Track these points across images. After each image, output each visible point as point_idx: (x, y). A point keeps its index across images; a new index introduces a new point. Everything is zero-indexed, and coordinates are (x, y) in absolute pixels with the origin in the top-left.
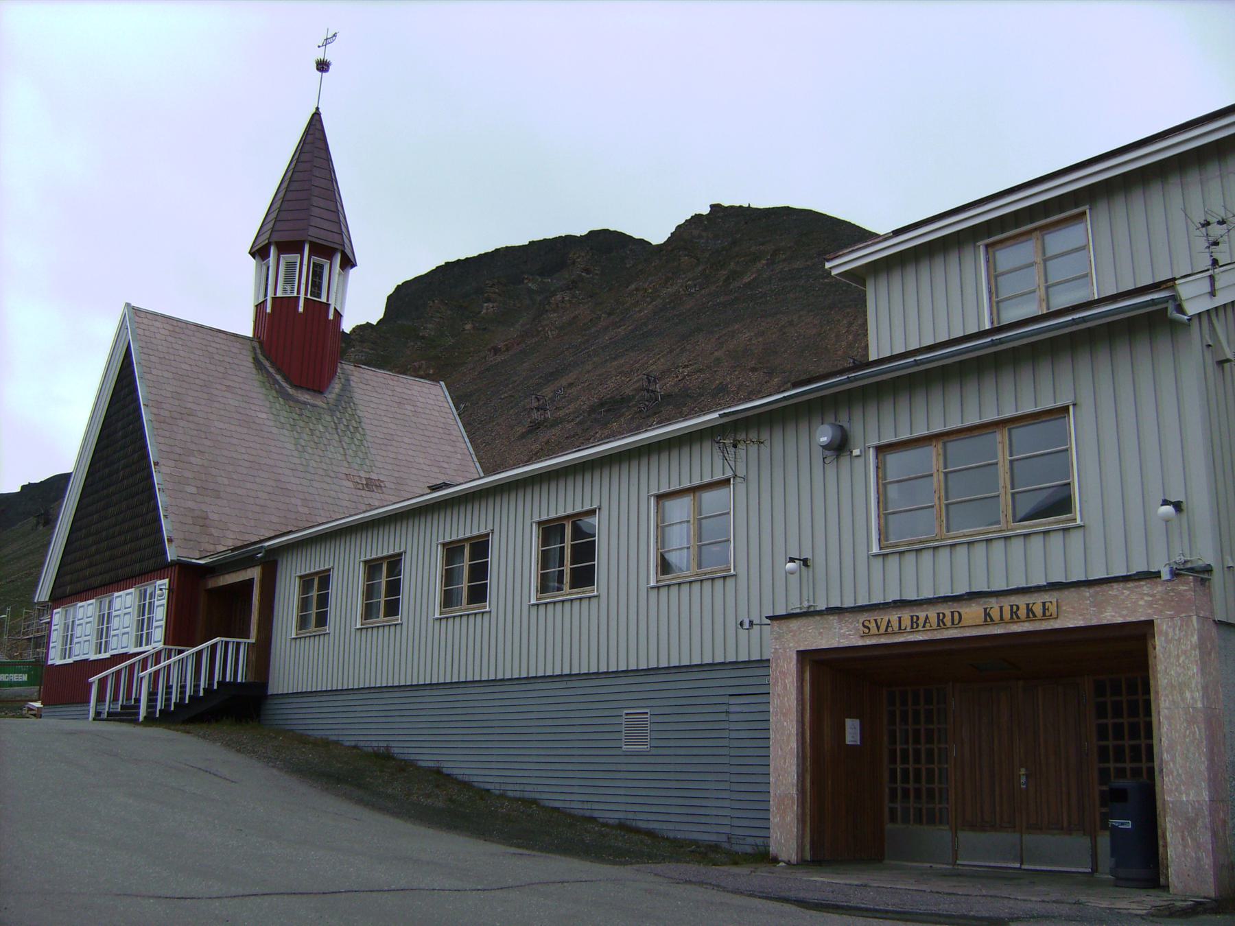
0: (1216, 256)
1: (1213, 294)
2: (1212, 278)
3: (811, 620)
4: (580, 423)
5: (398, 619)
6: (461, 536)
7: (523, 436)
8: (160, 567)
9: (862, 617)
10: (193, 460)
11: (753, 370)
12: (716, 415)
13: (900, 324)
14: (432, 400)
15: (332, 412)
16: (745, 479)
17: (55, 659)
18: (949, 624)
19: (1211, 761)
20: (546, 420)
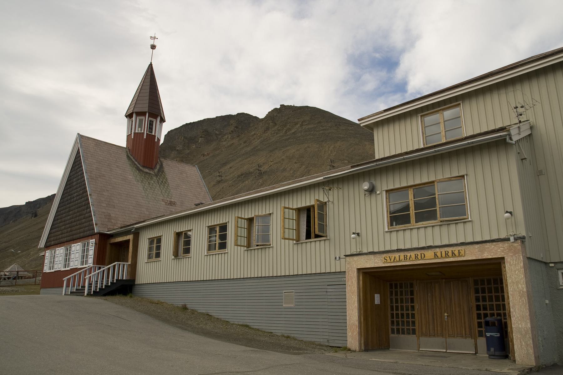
0: (520, 119)
1: (519, 134)
2: (519, 127)
3: (362, 256)
4: (234, 181)
5: (190, 255)
6: (216, 223)
7: (214, 185)
8: (92, 235)
9: (385, 255)
10: (104, 193)
11: (296, 163)
12: (322, 178)
13: (386, 145)
14: (192, 172)
15: (156, 176)
16: (333, 202)
17: (46, 270)
18: (420, 258)
19: (530, 311)
20: (222, 180)
